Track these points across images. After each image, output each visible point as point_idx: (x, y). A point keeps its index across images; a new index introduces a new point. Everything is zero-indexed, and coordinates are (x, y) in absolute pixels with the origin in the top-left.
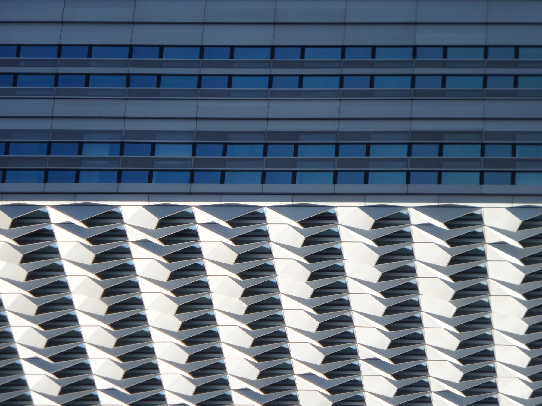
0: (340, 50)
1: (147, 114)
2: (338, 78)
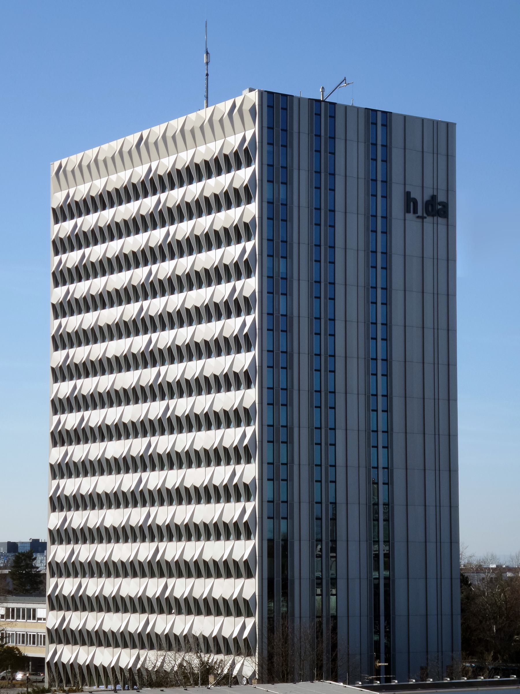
0: (333, 354)
1: (301, 291)
2: (320, 464)
